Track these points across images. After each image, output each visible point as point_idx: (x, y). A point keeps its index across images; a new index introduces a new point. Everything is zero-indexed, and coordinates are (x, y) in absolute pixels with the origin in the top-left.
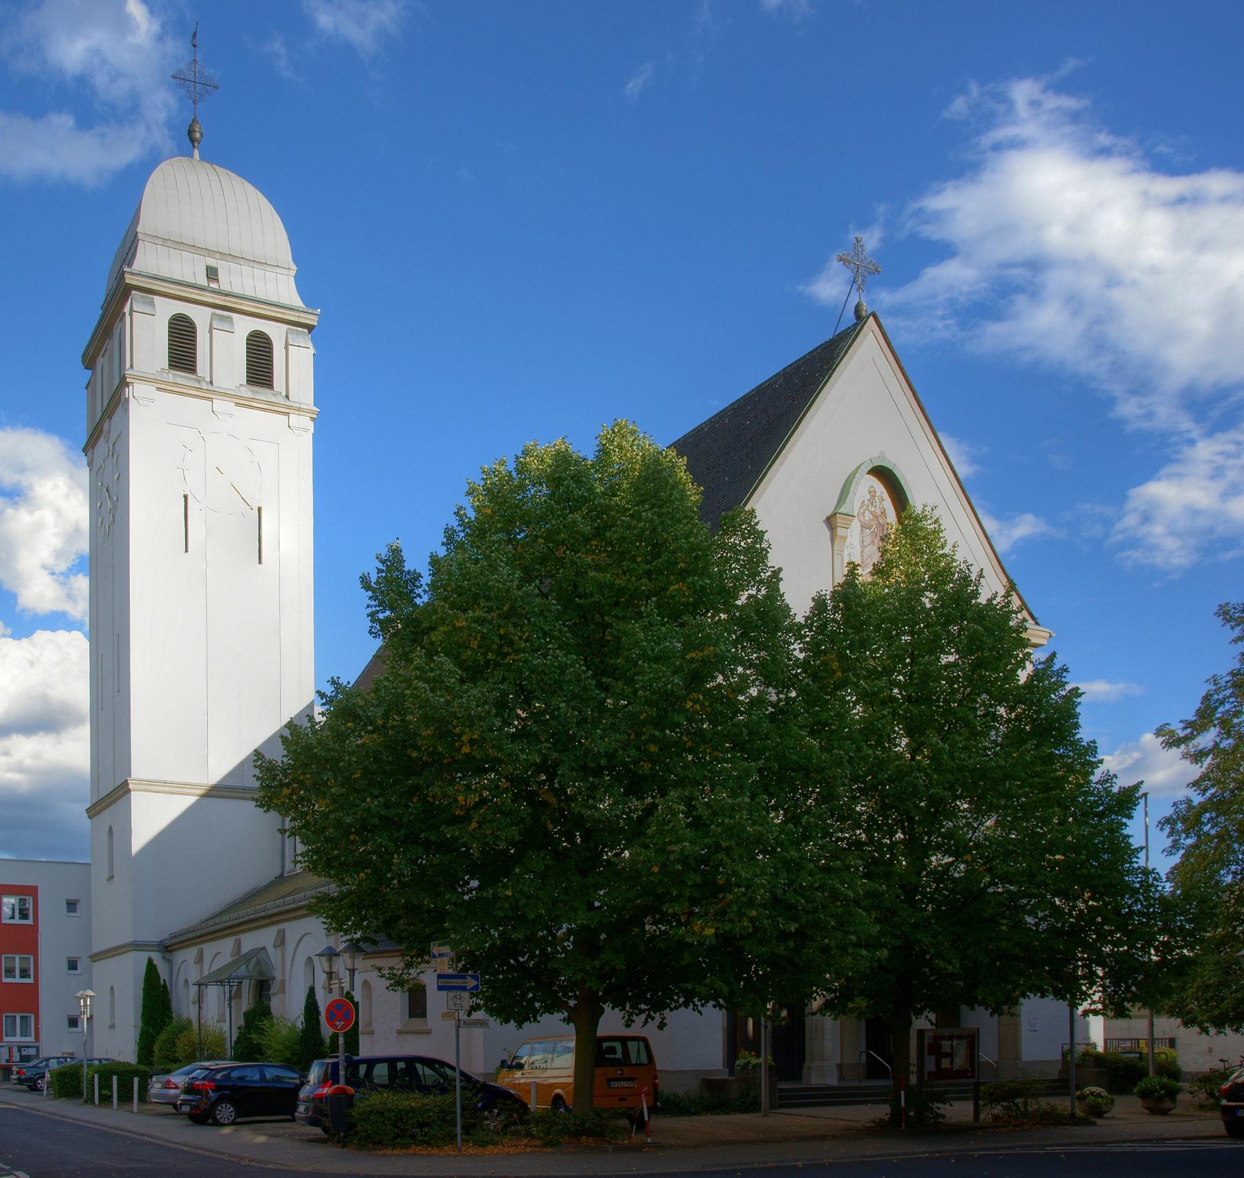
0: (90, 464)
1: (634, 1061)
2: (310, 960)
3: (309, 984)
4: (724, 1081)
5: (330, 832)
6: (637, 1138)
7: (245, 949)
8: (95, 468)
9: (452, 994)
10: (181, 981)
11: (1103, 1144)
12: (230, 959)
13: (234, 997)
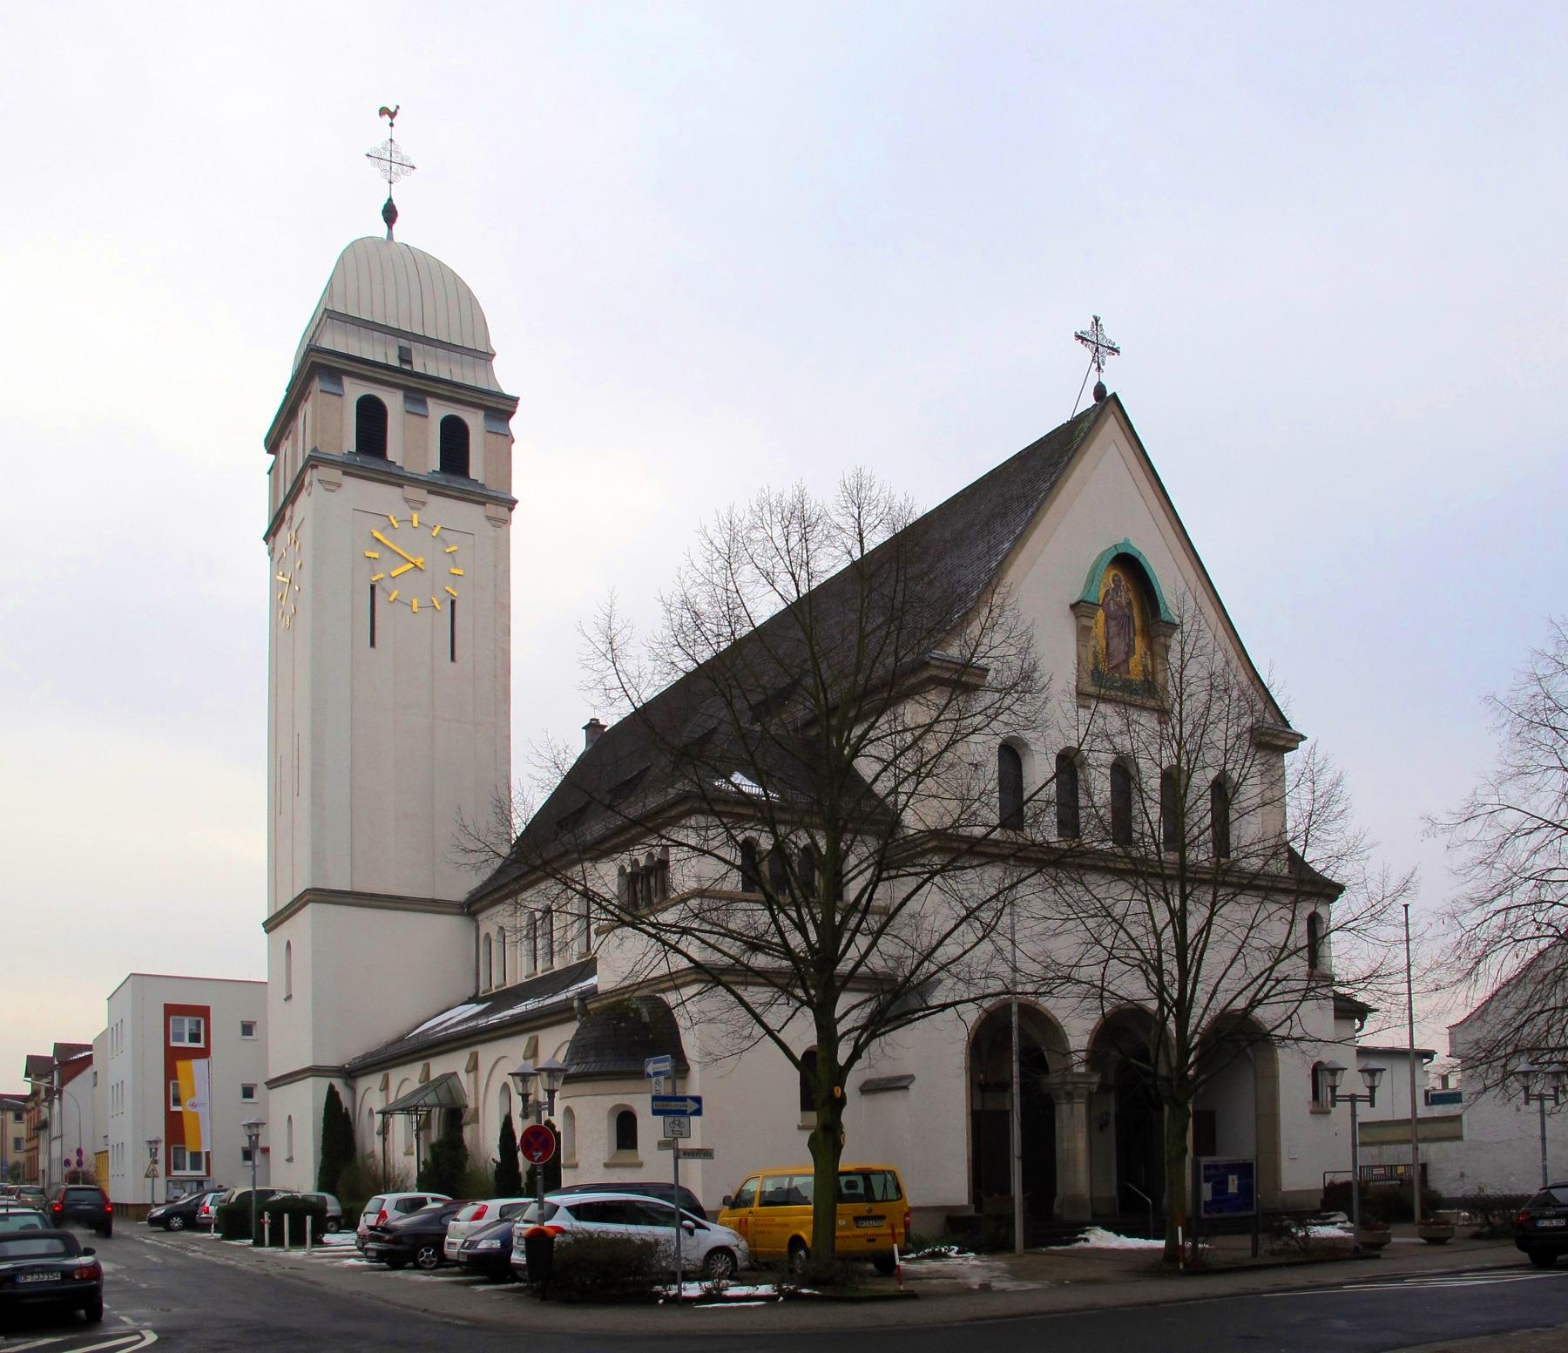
0: (271, 552)
1: (878, 1196)
2: (505, 1086)
3: (506, 1111)
4: (970, 1218)
5: (563, 756)
6: (890, 1286)
7: (434, 1075)
8: (277, 556)
9: (670, 1119)
10: (365, 1112)
11: (1401, 1280)
12: (418, 1085)
13: (423, 1126)
